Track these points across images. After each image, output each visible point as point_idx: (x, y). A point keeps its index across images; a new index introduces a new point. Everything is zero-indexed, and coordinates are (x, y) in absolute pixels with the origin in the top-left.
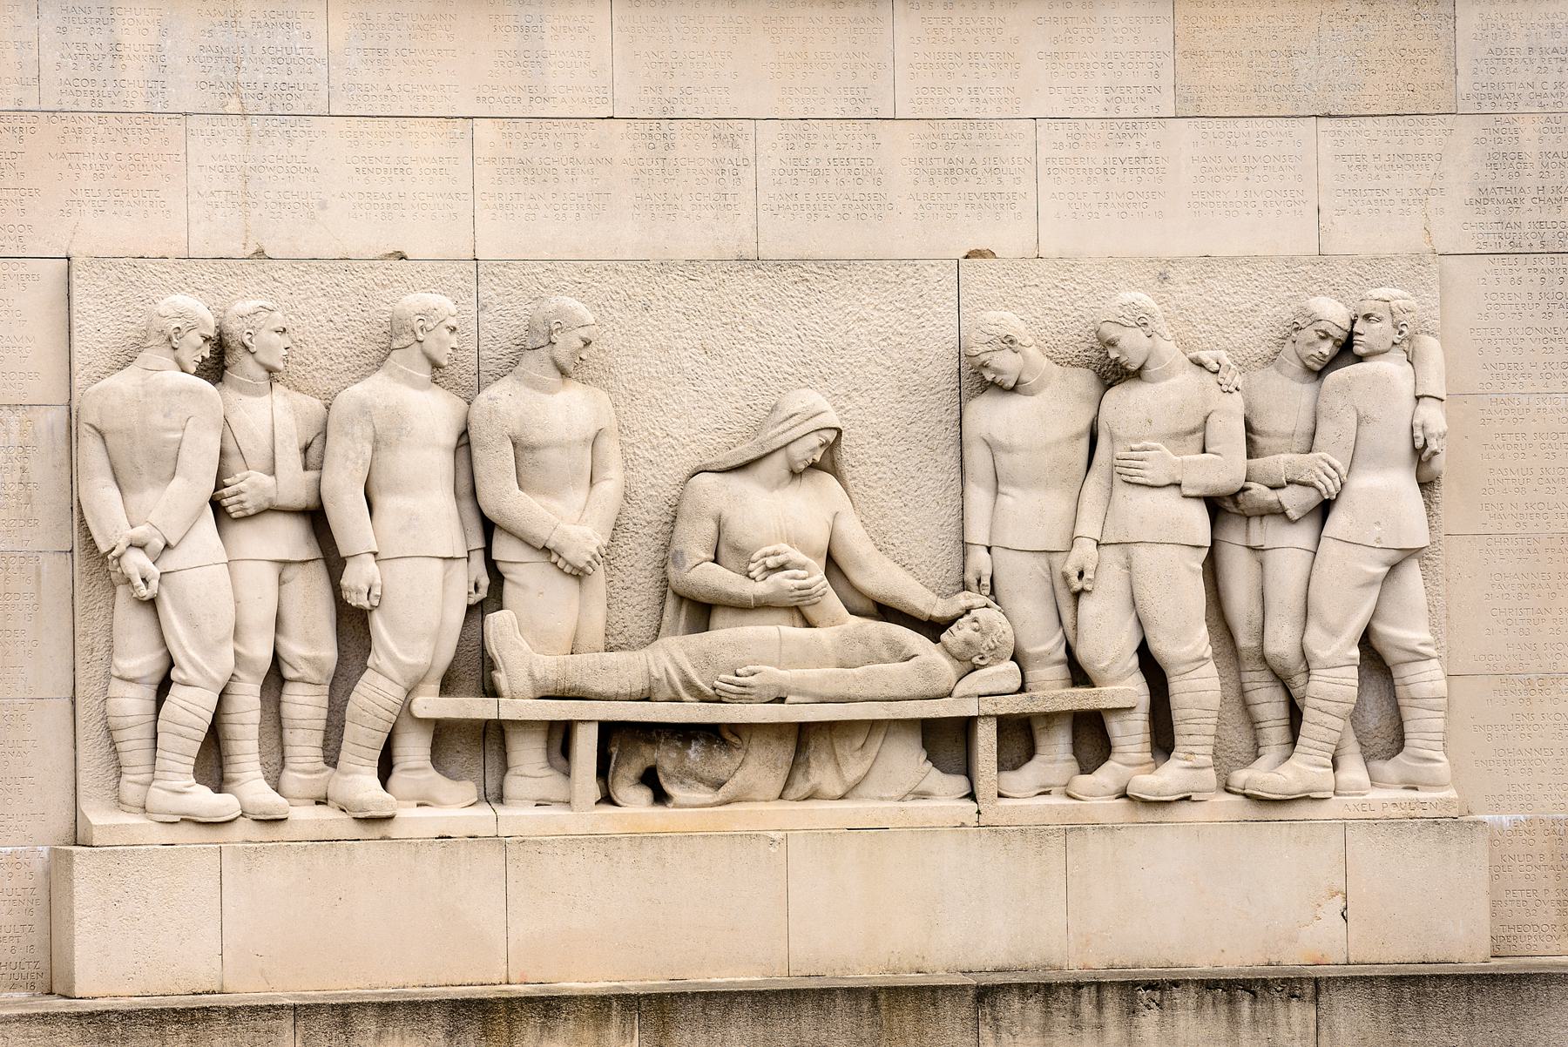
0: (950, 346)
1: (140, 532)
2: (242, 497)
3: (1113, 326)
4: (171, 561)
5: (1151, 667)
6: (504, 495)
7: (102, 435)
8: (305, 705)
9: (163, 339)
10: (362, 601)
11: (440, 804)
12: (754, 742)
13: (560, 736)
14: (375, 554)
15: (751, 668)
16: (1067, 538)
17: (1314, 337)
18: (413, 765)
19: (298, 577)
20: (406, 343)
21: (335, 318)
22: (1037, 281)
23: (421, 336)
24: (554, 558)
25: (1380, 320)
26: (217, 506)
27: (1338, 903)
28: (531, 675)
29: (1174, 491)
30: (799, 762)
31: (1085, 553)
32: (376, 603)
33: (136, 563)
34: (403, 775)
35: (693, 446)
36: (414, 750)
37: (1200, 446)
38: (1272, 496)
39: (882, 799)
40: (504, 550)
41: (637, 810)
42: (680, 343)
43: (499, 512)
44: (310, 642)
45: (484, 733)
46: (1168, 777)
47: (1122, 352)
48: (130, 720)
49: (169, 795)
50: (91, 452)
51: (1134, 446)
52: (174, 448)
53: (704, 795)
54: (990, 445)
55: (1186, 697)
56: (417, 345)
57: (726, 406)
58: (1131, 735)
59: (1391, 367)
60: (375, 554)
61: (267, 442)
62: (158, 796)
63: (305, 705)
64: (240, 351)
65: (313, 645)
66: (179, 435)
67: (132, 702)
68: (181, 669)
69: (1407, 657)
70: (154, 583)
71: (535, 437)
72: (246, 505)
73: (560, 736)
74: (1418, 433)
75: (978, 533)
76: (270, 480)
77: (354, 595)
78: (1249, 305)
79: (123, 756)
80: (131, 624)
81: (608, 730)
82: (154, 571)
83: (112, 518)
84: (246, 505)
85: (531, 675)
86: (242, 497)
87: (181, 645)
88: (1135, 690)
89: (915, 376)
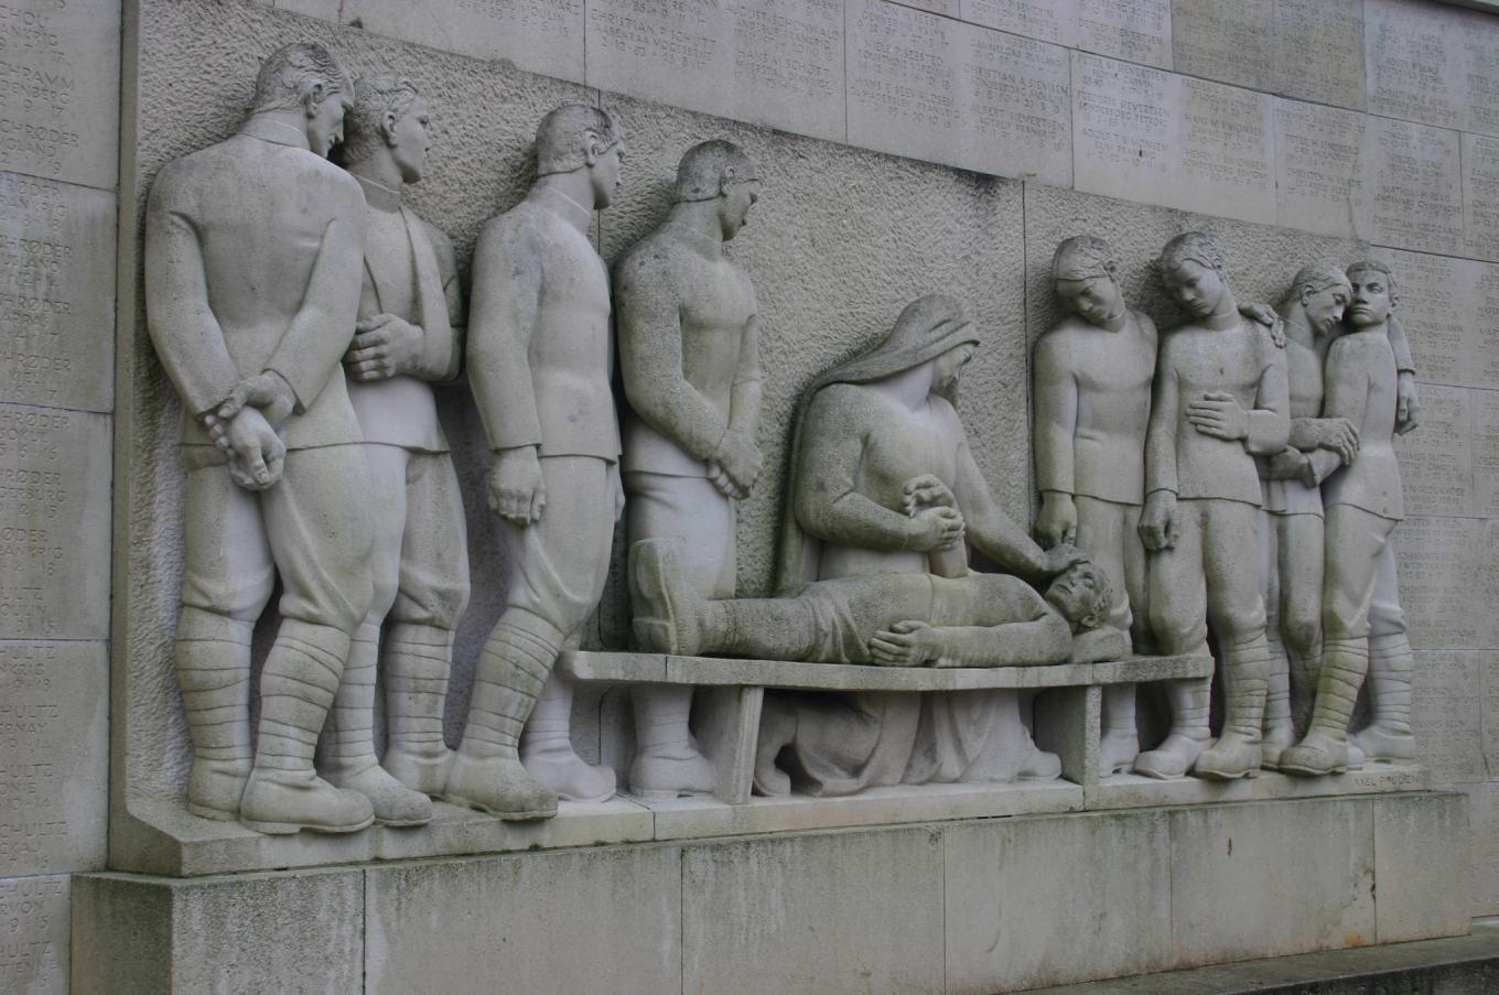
0: (1019, 273)
1: (263, 383)
2: (384, 349)
3: (1196, 266)
4: (303, 433)
5: (1220, 633)
6: (664, 381)
7: (200, 232)
8: (426, 655)
9: (296, 98)
10: (512, 510)
11: (579, 796)
12: (889, 714)
13: (705, 707)
14: (538, 446)
15: (912, 623)
16: (1141, 496)
17: (1332, 301)
18: (555, 743)
19: (428, 468)
20: (573, 165)
21: (451, 130)
22: (1085, 216)
23: (592, 159)
24: (715, 472)
25: (1381, 291)
26: (349, 364)
27: (1368, 880)
28: (701, 624)
29: (1238, 447)
30: (924, 743)
31: (1165, 505)
32: (537, 515)
33: (252, 428)
34: (542, 758)
35: (803, 354)
36: (556, 721)
37: (1253, 401)
38: (1304, 459)
39: (992, 780)
40: (655, 457)
41: (781, 803)
42: (791, 230)
43: (666, 405)
44: (441, 567)
45: (602, 702)
46: (1235, 750)
47: (1200, 294)
48: (226, 675)
49: (287, 792)
50: (180, 259)
51: (1211, 395)
52: (305, 263)
53: (844, 782)
54: (1081, 383)
55: (1253, 665)
56: (585, 171)
57: (832, 311)
58: (1195, 709)
59: (1377, 336)
60: (538, 446)
61: (406, 274)
62: (268, 793)
63: (426, 655)
64: (375, 141)
65: (448, 572)
66: (315, 245)
67: (228, 644)
68: (306, 595)
69: (1390, 628)
70: (279, 464)
71: (706, 312)
72: (386, 361)
73: (705, 707)
74: (1404, 406)
75: (1063, 479)
76: (416, 331)
77: (514, 504)
78: (1241, 268)
79: (262, 739)
80: (233, 528)
81: (779, 699)
82: (279, 444)
83: (206, 353)
84: (386, 361)
85: (701, 624)
86: (384, 349)
87: (310, 561)
88: (1199, 660)
89: (991, 303)
